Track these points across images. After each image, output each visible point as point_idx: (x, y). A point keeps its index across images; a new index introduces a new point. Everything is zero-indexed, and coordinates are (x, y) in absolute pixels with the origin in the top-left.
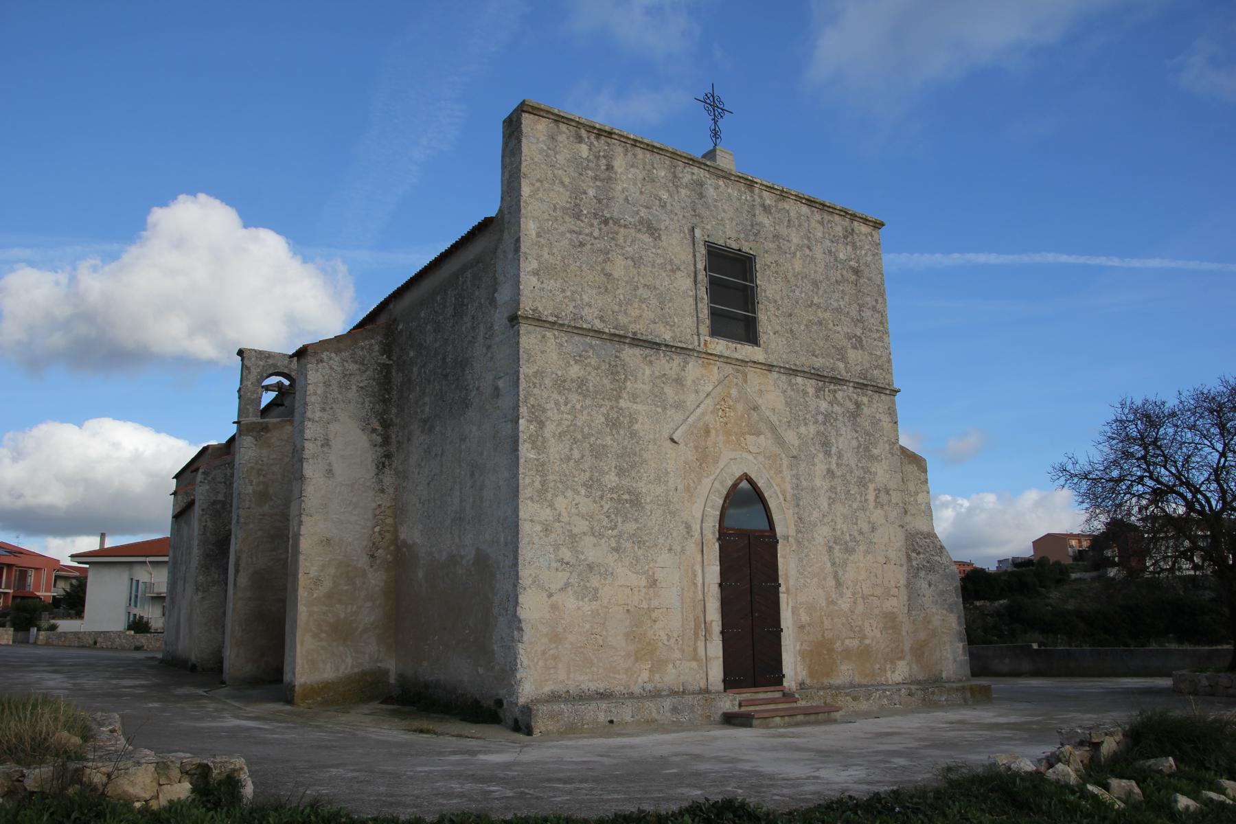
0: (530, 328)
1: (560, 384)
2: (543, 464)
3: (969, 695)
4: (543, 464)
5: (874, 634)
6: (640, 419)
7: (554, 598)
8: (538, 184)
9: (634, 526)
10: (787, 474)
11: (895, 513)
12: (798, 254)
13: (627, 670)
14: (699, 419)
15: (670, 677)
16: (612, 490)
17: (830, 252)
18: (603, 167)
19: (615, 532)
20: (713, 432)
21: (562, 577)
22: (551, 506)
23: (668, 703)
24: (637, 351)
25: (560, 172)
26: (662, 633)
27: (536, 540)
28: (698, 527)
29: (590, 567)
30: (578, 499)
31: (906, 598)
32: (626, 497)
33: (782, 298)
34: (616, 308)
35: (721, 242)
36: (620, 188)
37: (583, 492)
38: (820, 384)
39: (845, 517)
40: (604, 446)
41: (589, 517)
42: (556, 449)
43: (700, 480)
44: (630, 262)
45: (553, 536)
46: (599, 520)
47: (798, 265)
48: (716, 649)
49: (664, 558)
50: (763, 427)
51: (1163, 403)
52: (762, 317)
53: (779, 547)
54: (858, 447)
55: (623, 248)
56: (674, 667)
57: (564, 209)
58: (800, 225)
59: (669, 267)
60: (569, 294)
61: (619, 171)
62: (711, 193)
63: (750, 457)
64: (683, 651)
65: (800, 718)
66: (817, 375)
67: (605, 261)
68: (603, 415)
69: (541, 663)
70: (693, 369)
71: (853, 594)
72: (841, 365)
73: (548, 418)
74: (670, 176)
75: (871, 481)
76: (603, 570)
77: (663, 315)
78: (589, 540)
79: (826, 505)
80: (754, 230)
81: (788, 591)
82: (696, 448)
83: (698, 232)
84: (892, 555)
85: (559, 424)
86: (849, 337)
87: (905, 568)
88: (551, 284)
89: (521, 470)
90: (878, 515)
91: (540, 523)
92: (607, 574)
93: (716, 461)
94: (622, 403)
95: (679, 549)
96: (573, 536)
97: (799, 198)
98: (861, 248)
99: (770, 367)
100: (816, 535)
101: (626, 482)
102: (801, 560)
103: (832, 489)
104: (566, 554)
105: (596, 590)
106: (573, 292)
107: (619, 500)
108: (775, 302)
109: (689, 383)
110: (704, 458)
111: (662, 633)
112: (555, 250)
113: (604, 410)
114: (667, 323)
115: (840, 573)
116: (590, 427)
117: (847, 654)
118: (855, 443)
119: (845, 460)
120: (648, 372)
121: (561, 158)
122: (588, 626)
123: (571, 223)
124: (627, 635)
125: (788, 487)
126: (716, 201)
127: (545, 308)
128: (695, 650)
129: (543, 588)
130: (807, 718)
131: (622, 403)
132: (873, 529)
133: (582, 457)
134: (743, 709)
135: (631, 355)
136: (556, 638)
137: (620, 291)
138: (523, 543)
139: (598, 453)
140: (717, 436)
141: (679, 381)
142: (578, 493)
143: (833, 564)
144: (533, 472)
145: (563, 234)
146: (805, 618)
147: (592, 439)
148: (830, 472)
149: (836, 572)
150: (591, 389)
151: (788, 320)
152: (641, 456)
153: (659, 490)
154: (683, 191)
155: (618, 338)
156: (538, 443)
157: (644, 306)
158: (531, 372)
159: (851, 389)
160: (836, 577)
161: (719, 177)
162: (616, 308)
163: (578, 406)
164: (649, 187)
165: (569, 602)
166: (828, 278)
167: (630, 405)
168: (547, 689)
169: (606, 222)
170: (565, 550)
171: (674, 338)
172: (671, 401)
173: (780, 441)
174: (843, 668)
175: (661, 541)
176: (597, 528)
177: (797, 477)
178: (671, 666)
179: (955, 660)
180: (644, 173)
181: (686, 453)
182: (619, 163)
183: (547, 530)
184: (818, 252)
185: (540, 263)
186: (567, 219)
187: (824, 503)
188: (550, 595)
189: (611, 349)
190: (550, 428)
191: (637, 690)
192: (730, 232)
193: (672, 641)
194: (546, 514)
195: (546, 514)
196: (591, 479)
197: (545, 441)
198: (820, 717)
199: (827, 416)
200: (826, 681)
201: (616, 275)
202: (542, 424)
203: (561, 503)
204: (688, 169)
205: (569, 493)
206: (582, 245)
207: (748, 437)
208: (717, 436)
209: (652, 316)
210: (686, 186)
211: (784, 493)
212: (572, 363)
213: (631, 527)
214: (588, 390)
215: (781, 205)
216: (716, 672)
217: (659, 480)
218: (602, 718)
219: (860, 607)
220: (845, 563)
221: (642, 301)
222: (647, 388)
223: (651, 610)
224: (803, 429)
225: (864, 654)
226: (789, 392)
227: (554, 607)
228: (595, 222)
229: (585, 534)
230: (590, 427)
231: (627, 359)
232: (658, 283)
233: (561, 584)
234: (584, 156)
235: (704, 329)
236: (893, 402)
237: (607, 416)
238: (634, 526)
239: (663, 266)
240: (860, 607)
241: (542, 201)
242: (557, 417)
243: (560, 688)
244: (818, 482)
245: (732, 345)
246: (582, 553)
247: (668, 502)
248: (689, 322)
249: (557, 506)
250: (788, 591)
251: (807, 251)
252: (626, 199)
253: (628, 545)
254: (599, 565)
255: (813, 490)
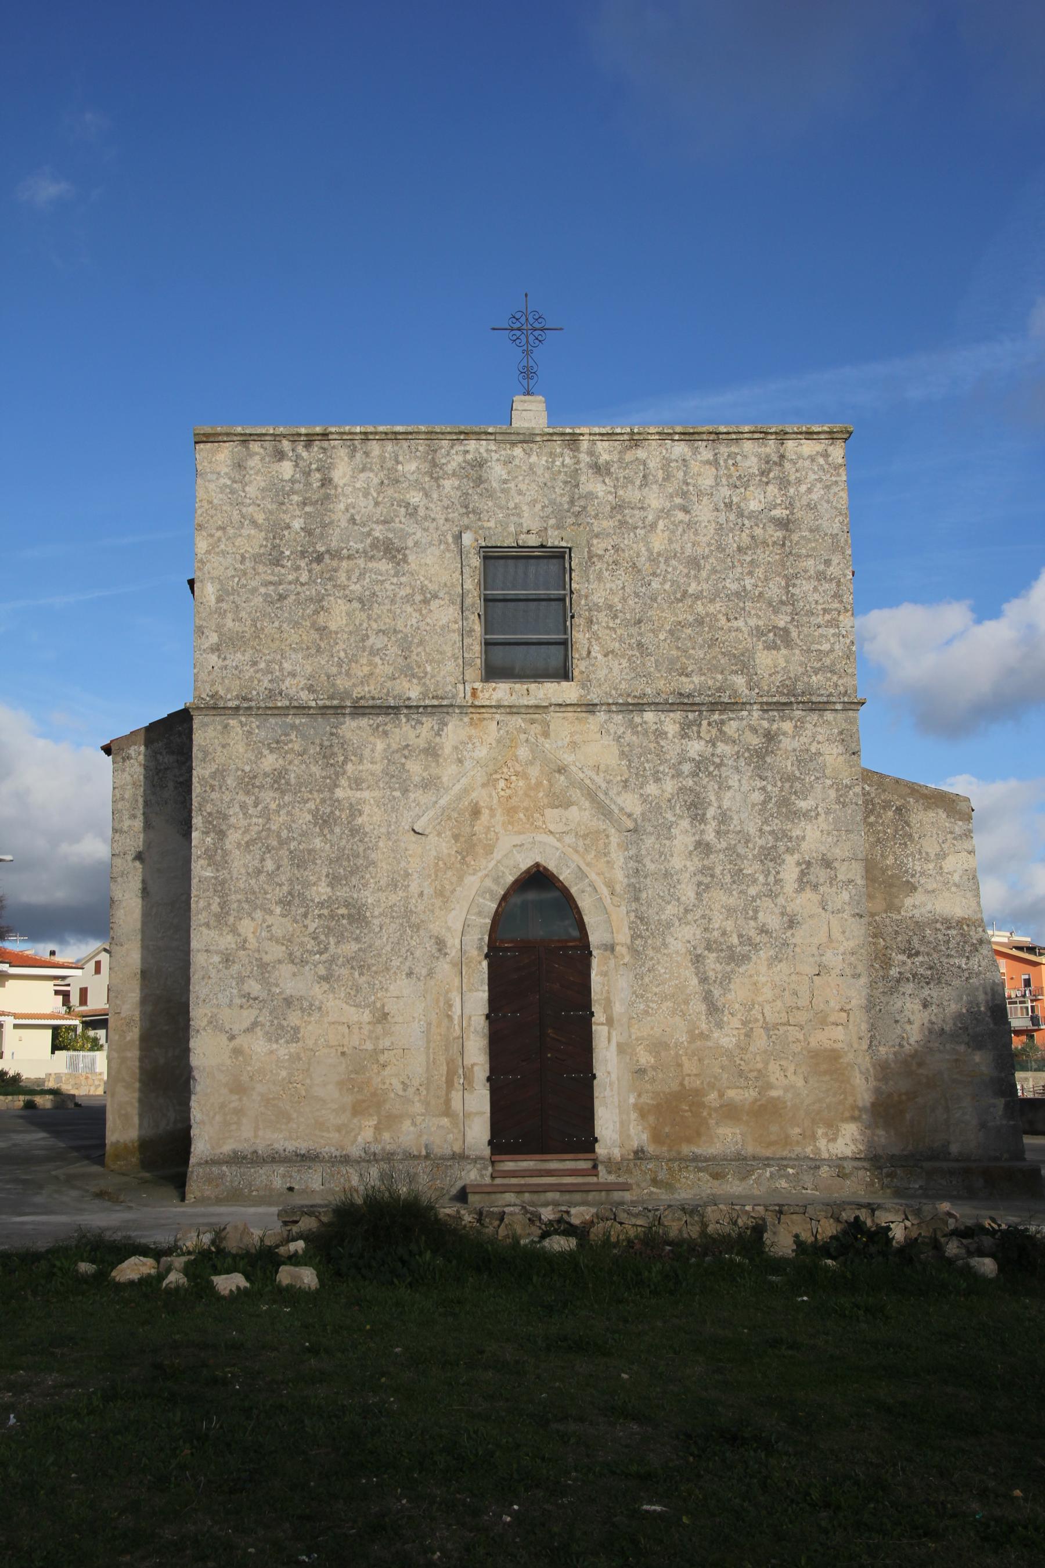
0: (206, 719)
1: (249, 783)
2: (223, 883)
4: (223, 883)
5: (788, 1081)
6: (367, 809)
7: (236, 1042)
8: (219, 533)
9: (354, 946)
10: (618, 857)
12: (661, 524)
13: (339, 1129)
14: (459, 798)
16: (321, 905)
17: (729, 506)
18: (316, 485)
19: (324, 957)
20: (486, 812)
21: (248, 1016)
22: (234, 931)
24: (364, 722)
25: (251, 509)
27: (213, 973)
28: (457, 942)
29: (288, 1002)
30: (270, 920)
31: (864, 1026)
32: (343, 911)
33: (624, 600)
35: (510, 542)
36: (342, 506)
39: (730, 911)
40: (310, 851)
41: (288, 940)
42: (240, 863)
43: (461, 879)
44: (356, 605)
47: (658, 542)
50: (576, 794)
52: (580, 637)
53: (595, 962)
54: (764, 803)
56: (414, 1124)
57: (257, 558)
58: (667, 478)
59: (418, 598)
60: (262, 665)
61: (341, 483)
62: (497, 471)
63: (551, 840)
64: (427, 1104)
67: (316, 612)
68: (310, 811)
70: (455, 731)
73: (230, 826)
74: (425, 467)
76: (305, 1004)
77: (409, 667)
78: (286, 969)
79: (692, 895)
80: (577, 507)
81: (610, 1022)
82: (456, 837)
83: (467, 539)
85: (247, 831)
86: (759, 633)
87: (863, 980)
88: (238, 658)
89: (194, 893)
90: (805, 902)
91: (217, 952)
92: (311, 1008)
93: (489, 850)
94: (339, 793)
95: (424, 972)
96: (263, 966)
98: (799, 482)
99: (590, 708)
100: (670, 940)
101: (342, 893)
103: (706, 870)
104: (254, 987)
105: (296, 1030)
106: (268, 663)
108: (610, 607)
109: (448, 750)
110: (469, 848)
111: (395, 1081)
112: (243, 614)
113: (311, 805)
114: (413, 676)
115: (717, 992)
116: (290, 829)
117: (730, 1112)
118: (757, 797)
120: (380, 746)
121: (251, 490)
122: (284, 1073)
123: (266, 573)
124: (340, 1084)
125: (619, 875)
126: (505, 482)
127: (229, 690)
128: (448, 1102)
129: (222, 1030)
131: (339, 793)
133: (278, 868)
134: (498, 1181)
135: (352, 728)
136: (238, 1088)
137: (341, 646)
138: (195, 978)
139: (301, 860)
140: (492, 815)
141: (431, 752)
142: (271, 912)
143: (704, 980)
144: (210, 893)
145: (254, 590)
146: (645, 1059)
147: (293, 845)
148: (703, 847)
149: (709, 992)
150: (293, 781)
151: (633, 630)
152: (366, 857)
153: (394, 898)
154: (448, 484)
155: (334, 710)
156: (217, 858)
157: (377, 660)
158: (207, 773)
159: (756, 714)
160: (707, 997)
161: (513, 444)
162: (334, 670)
163: (273, 806)
164: (390, 492)
165: (258, 1046)
166: (720, 548)
167: (350, 793)
168: (227, 1148)
169: (319, 559)
170: (252, 983)
171: (424, 695)
172: (417, 779)
173: (604, 811)
175: (396, 963)
176: (298, 954)
177: (638, 859)
178: (408, 1122)
179: (983, 1125)
180: (382, 475)
181: (441, 845)
182: (341, 472)
183: (227, 960)
184: (703, 512)
185: (221, 635)
186: (261, 568)
187: (688, 893)
188: (232, 1038)
190: (233, 837)
194: (227, 941)
195: (227, 941)
196: (290, 893)
197: (226, 853)
199: (700, 765)
200: (686, 1150)
201: (333, 626)
202: (222, 834)
203: (246, 927)
204: (459, 448)
206: (282, 597)
207: (548, 812)
208: (492, 815)
209: (389, 670)
210: (454, 474)
211: (610, 885)
212: (266, 752)
213: (350, 948)
214: (288, 783)
215: (629, 456)
216: (478, 1132)
217: (394, 885)
219: (760, 1041)
220: (727, 978)
221: (374, 652)
222: (378, 768)
223: (377, 1052)
224: (652, 789)
225: (766, 1111)
226: (629, 737)
227: (237, 1052)
228: (303, 564)
229: (280, 962)
230: (290, 829)
231: (349, 735)
233: (246, 1024)
234: (287, 477)
235: (474, 673)
236: (852, 722)
237: (315, 814)
238: (354, 946)
239: (408, 599)
240: (760, 1041)
241: (224, 553)
242: (243, 823)
244: (677, 863)
246: (277, 985)
247: (408, 913)
248: (450, 666)
249: (241, 930)
251: (680, 516)
252: (352, 520)
253: (345, 971)
254: (300, 999)
255: (667, 875)
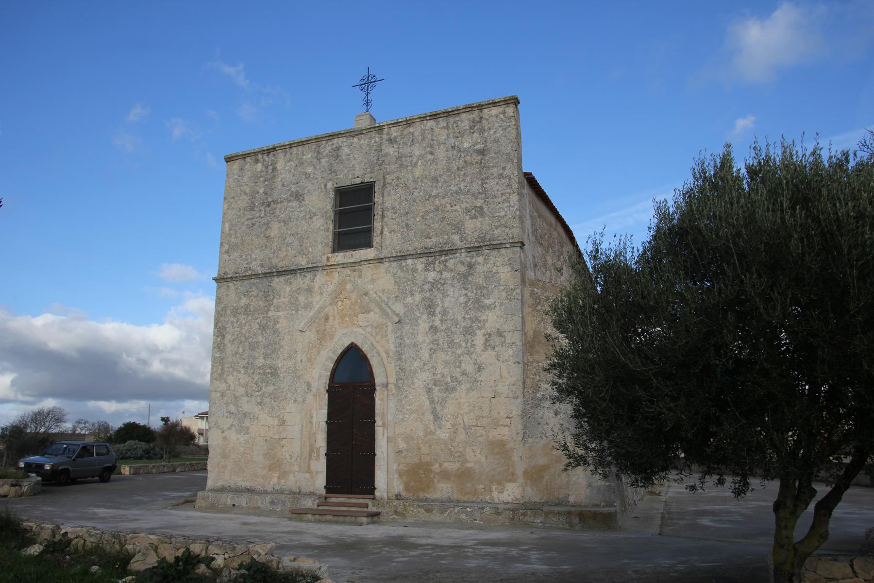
3: (577, 520)
4: (223, 359)
5: (477, 458)
6: (281, 321)
10: (391, 337)
11: (510, 352)
15: (291, 482)
16: (260, 368)
19: (260, 393)
20: (331, 318)
22: (226, 382)
23: (268, 498)
24: (282, 278)
26: (287, 455)
29: (245, 415)
31: (520, 427)
32: (269, 371)
34: (272, 255)
37: (243, 371)
38: (430, 259)
41: (246, 385)
43: (319, 352)
44: (282, 224)
45: (226, 398)
46: (251, 387)
48: (320, 466)
49: (291, 407)
51: (726, 162)
55: (278, 216)
63: (360, 330)
65: (331, 517)
66: (426, 253)
69: (217, 470)
71: (453, 426)
72: (456, 238)
74: (315, 155)
75: (479, 328)
77: (302, 250)
78: (245, 399)
79: (427, 355)
82: (318, 332)
84: (502, 388)
90: (487, 357)
92: (254, 418)
94: (270, 314)
95: (301, 400)
96: (236, 398)
97: (423, 118)
100: (416, 380)
102: (400, 401)
103: (435, 342)
104: (232, 408)
105: (248, 428)
107: (264, 373)
109: (316, 288)
110: (323, 336)
111: (287, 455)
113: (258, 320)
115: (438, 408)
117: (445, 475)
118: (462, 299)
119: (450, 315)
120: (288, 290)
122: (242, 449)
125: (392, 347)
129: (220, 428)
130: (336, 518)
132: (480, 369)
134: (320, 508)
139: (253, 347)
140: (334, 320)
142: (240, 372)
143: (432, 402)
146: (402, 445)
148: (433, 329)
157: (289, 248)
160: (434, 412)
161: (354, 136)
162: (272, 255)
165: (233, 436)
168: (219, 484)
169: (269, 205)
174: (441, 485)
181: (311, 336)
183: (223, 395)
184: (441, 153)
186: (246, 213)
187: (425, 354)
188: (223, 432)
189: (265, 282)
190: (228, 337)
191: (269, 489)
192: (358, 172)
193: (293, 459)
197: (225, 345)
198: (347, 519)
199: (434, 285)
200: (422, 495)
202: (224, 336)
203: (230, 379)
205: (235, 373)
206: (253, 225)
208: (334, 320)
211: (387, 352)
213: (271, 388)
216: (320, 482)
218: (229, 502)
219: (462, 436)
223: (280, 439)
224: (409, 300)
225: (464, 475)
227: (225, 438)
232: (299, 231)
233: (228, 426)
243: (226, 484)
244: (420, 338)
245: (348, 254)
250: (384, 425)
255: (415, 345)
